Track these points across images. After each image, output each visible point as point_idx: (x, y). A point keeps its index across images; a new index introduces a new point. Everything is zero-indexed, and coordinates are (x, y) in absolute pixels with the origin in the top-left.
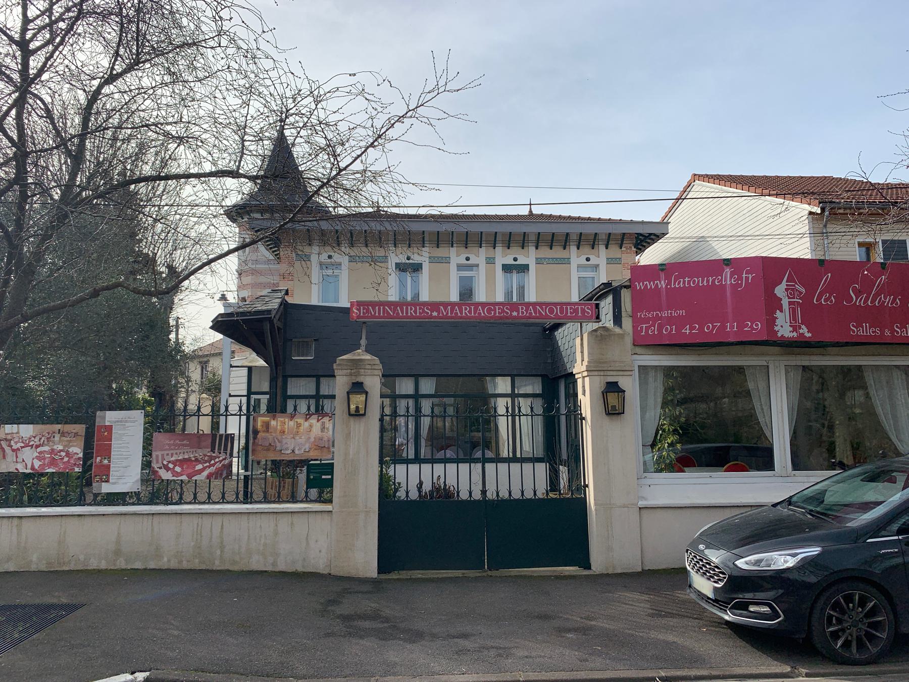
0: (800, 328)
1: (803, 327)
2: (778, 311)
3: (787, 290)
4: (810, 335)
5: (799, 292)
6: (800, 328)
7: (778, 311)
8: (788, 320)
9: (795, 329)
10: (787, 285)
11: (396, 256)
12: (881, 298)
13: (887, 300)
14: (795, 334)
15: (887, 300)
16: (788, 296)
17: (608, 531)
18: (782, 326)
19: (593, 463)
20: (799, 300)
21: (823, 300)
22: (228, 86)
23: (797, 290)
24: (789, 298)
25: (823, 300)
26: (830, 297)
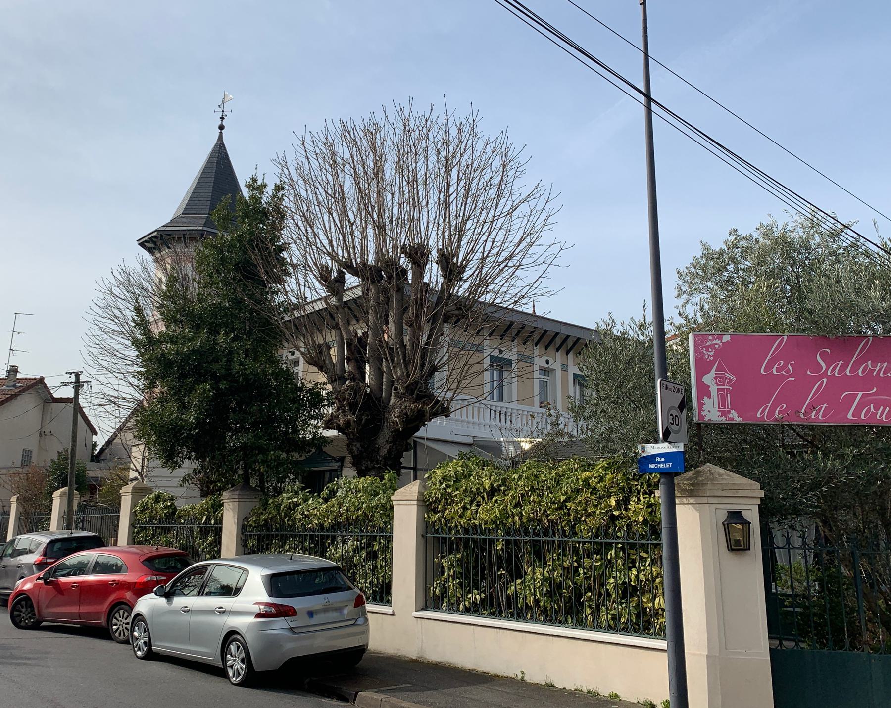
0: (729, 412)
1: (733, 411)
2: (705, 398)
3: (715, 378)
4: (740, 419)
5: (729, 379)
6: (729, 412)
7: (705, 398)
8: (716, 406)
9: (723, 413)
10: (716, 374)
11: (490, 347)
12: (867, 365)
13: (878, 368)
14: (723, 418)
15: (878, 368)
16: (716, 383)
17: (498, 690)
18: (709, 411)
19: (7, 533)
20: (729, 387)
21: (774, 369)
22: (326, 157)
23: (726, 378)
24: (718, 385)
25: (774, 369)
26: (785, 366)
